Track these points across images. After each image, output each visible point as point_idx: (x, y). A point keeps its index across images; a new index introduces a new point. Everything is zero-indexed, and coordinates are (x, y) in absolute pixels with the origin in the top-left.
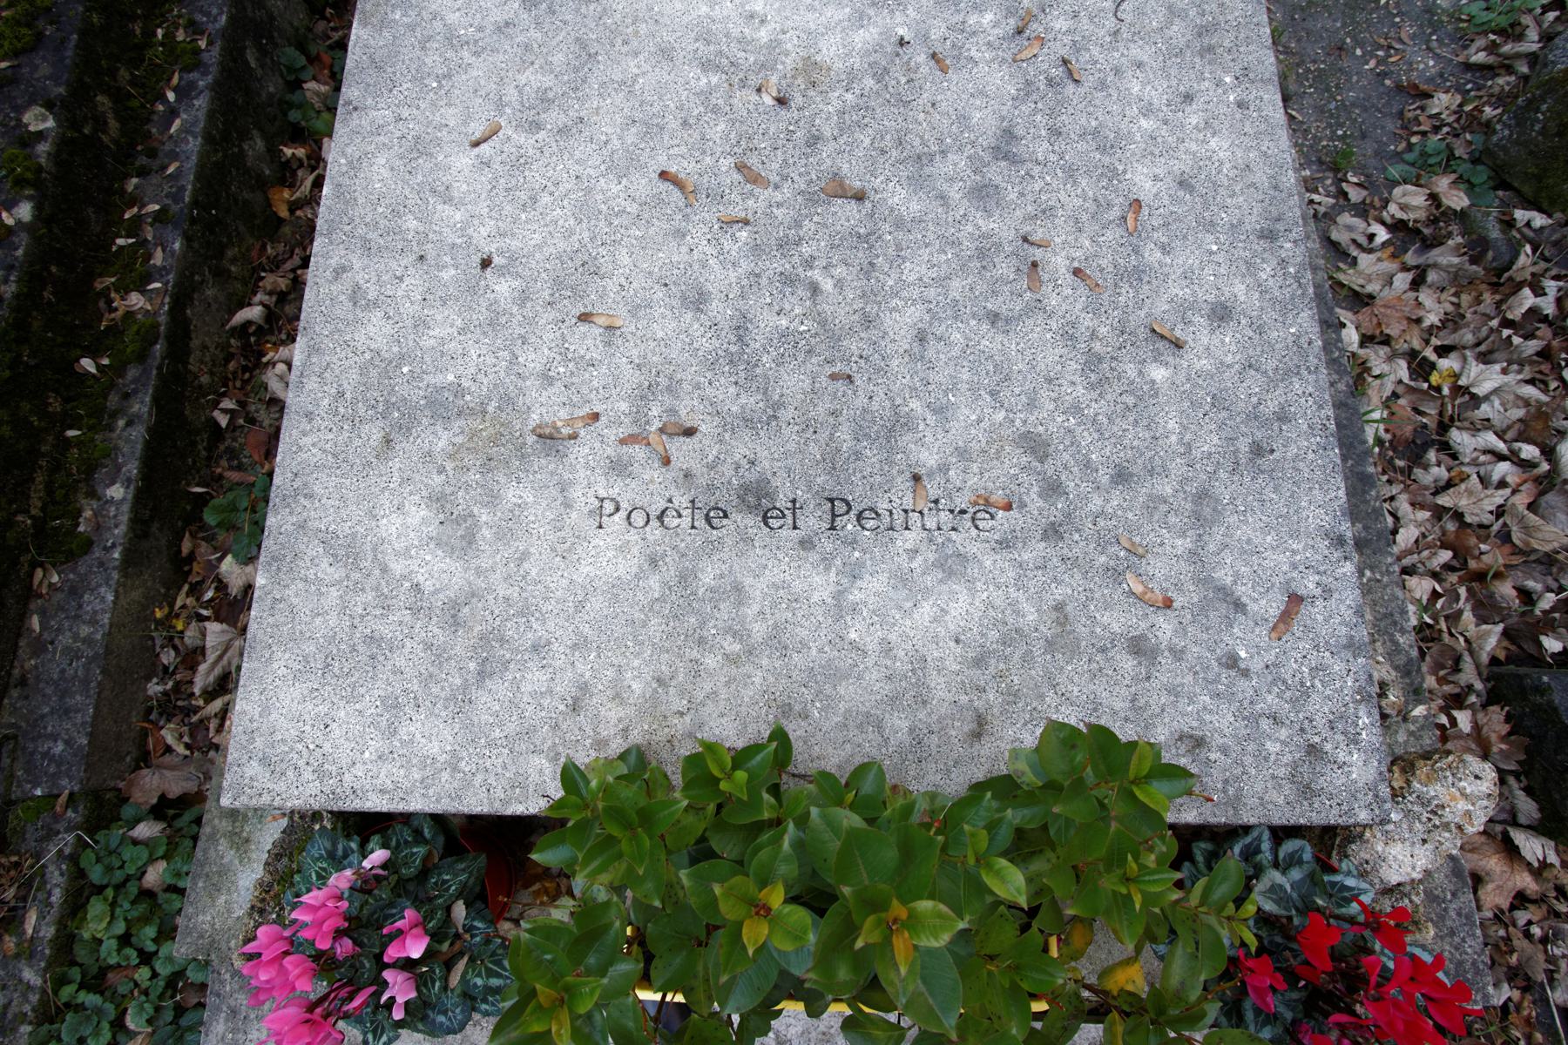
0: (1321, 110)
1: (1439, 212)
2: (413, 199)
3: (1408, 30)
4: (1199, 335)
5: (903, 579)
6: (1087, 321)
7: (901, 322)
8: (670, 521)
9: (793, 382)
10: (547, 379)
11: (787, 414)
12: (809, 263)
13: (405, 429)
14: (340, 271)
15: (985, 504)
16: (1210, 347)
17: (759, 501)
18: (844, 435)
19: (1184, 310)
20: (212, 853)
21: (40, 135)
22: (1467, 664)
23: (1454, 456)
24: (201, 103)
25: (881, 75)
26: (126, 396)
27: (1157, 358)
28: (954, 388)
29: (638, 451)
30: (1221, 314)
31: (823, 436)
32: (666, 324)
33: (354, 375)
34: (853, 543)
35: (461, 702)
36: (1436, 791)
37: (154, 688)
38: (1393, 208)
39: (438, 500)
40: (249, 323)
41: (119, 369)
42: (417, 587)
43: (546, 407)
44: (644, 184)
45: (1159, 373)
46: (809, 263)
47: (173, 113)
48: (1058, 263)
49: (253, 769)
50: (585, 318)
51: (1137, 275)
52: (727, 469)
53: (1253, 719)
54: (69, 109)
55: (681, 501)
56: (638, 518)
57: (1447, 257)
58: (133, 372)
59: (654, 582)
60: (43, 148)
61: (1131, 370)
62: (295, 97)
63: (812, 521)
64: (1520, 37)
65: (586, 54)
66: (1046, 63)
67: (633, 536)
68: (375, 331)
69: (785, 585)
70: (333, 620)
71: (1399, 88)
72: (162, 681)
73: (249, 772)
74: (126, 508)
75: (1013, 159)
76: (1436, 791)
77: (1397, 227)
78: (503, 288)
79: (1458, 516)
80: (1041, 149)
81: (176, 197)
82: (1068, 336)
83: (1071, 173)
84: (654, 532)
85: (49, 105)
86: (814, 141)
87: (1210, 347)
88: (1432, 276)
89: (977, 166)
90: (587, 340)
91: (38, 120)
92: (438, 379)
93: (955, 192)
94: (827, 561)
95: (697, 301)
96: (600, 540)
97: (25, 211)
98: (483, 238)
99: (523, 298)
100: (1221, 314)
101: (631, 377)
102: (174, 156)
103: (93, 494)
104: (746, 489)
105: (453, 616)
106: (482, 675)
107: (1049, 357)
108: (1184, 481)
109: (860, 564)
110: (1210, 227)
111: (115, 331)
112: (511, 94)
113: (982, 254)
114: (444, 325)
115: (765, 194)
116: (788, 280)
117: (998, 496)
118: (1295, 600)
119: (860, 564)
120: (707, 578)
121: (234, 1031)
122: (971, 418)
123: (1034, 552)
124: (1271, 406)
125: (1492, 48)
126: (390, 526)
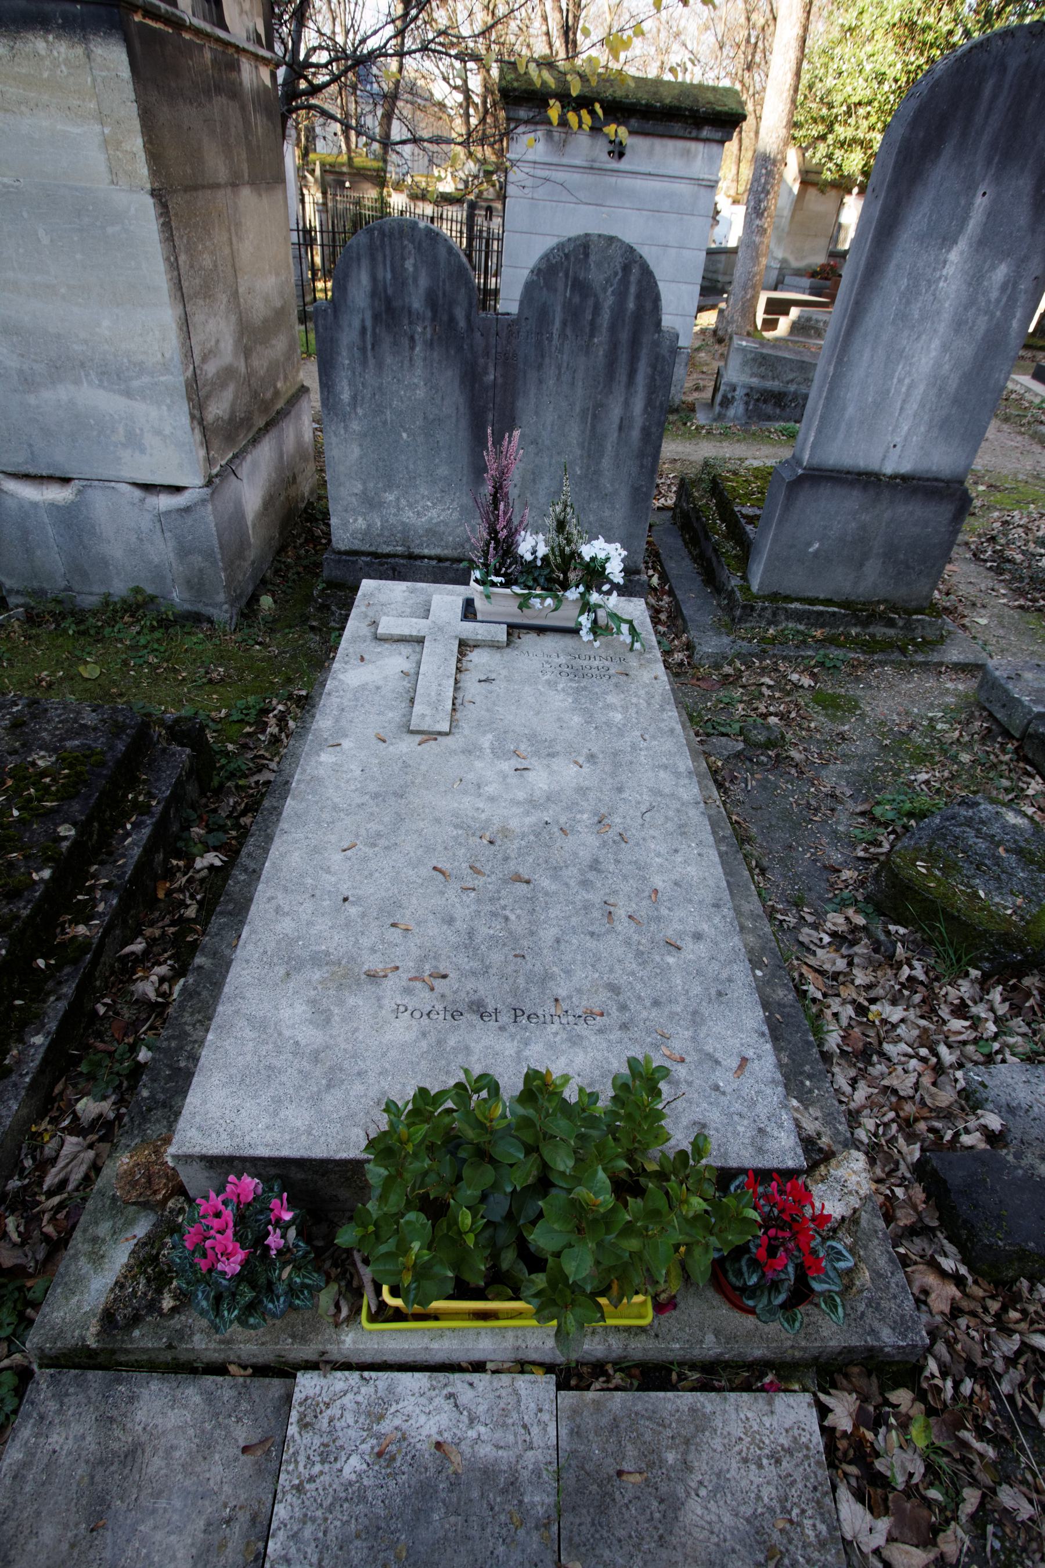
0: (784, 876)
1: (855, 929)
2: (311, 871)
3: (825, 840)
4: (688, 944)
5: (551, 1046)
6: (636, 937)
7: (548, 934)
8: (433, 1016)
9: (496, 957)
10: (373, 950)
11: (492, 971)
12: (504, 908)
13: (298, 969)
14: (270, 899)
15: (589, 1014)
16: (692, 950)
17: (479, 1009)
18: (521, 981)
19: (681, 934)
20: (73, 1267)
21: (66, 838)
22: (903, 1167)
23: (889, 1059)
24: (146, 831)
25: (537, 835)
26: (60, 983)
27: (669, 953)
28: (574, 962)
29: (418, 984)
30: (698, 937)
31: (511, 981)
32: (434, 930)
33: (273, 944)
34: (526, 1029)
35: (315, 1100)
36: (839, 1173)
37: (14, 1184)
38: (829, 925)
39: (312, 1002)
40: (133, 953)
41: (58, 967)
42: (297, 1043)
43: (373, 962)
44: (425, 871)
45: (671, 960)
46: (504, 908)
47: (128, 834)
48: (621, 913)
49: (193, 1132)
50: (394, 925)
51: (658, 919)
52: (463, 995)
53: (730, 1115)
54: (83, 829)
55: (439, 1007)
56: (417, 1014)
57: (861, 950)
58: (67, 970)
59: (424, 1044)
60: (65, 844)
61: (658, 958)
62: (185, 834)
63: (505, 1018)
64: (880, 845)
65: (400, 818)
66: (612, 834)
67: (414, 1022)
68: (286, 926)
69: (490, 1047)
70: (249, 1057)
71: (825, 867)
72: (21, 1178)
73: (189, 1134)
74: (42, 1050)
75: (599, 871)
76: (839, 1173)
77: (834, 934)
78: (353, 911)
79: (895, 1092)
80: (611, 868)
81: (119, 877)
82: (627, 942)
83: (625, 878)
84: (425, 1020)
85: (74, 824)
86: (506, 859)
87: (692, 950)
88: (856, 960)
89: (582, 872)
90: (395, 935)
91: (66, 830)
92: (317, 948)
93: (572, 883)
94: (512, 1037)
95: (450, 921)
96: (397, 1023)
97: (46, 874)
98: (345, 889)
99: (363, 915)
100: (698, 937)
101: (415, 952)
102: (124, 856)
103: (21, 1040)
104: (472, 1003)
105: (316, 1057)
106: (329, 1086)
107: (619, 951)
108: (686, 1006)
109: (529, 1038)
110: (690, 901)
111: (63, 945)
112: (363, 832)
113: (585, 908)
114: (322, 925)
115: (483, 879)
116: (494, 914)
117: (596, 1010)
118: (744, 1060)
119: (529, 1038)
120: (452, 1042)
121: (37, 1436)
122: (582, 975)
123: (615, 1035)
124: (724, 976)
125: (866, 850)
126: (285, 1013)
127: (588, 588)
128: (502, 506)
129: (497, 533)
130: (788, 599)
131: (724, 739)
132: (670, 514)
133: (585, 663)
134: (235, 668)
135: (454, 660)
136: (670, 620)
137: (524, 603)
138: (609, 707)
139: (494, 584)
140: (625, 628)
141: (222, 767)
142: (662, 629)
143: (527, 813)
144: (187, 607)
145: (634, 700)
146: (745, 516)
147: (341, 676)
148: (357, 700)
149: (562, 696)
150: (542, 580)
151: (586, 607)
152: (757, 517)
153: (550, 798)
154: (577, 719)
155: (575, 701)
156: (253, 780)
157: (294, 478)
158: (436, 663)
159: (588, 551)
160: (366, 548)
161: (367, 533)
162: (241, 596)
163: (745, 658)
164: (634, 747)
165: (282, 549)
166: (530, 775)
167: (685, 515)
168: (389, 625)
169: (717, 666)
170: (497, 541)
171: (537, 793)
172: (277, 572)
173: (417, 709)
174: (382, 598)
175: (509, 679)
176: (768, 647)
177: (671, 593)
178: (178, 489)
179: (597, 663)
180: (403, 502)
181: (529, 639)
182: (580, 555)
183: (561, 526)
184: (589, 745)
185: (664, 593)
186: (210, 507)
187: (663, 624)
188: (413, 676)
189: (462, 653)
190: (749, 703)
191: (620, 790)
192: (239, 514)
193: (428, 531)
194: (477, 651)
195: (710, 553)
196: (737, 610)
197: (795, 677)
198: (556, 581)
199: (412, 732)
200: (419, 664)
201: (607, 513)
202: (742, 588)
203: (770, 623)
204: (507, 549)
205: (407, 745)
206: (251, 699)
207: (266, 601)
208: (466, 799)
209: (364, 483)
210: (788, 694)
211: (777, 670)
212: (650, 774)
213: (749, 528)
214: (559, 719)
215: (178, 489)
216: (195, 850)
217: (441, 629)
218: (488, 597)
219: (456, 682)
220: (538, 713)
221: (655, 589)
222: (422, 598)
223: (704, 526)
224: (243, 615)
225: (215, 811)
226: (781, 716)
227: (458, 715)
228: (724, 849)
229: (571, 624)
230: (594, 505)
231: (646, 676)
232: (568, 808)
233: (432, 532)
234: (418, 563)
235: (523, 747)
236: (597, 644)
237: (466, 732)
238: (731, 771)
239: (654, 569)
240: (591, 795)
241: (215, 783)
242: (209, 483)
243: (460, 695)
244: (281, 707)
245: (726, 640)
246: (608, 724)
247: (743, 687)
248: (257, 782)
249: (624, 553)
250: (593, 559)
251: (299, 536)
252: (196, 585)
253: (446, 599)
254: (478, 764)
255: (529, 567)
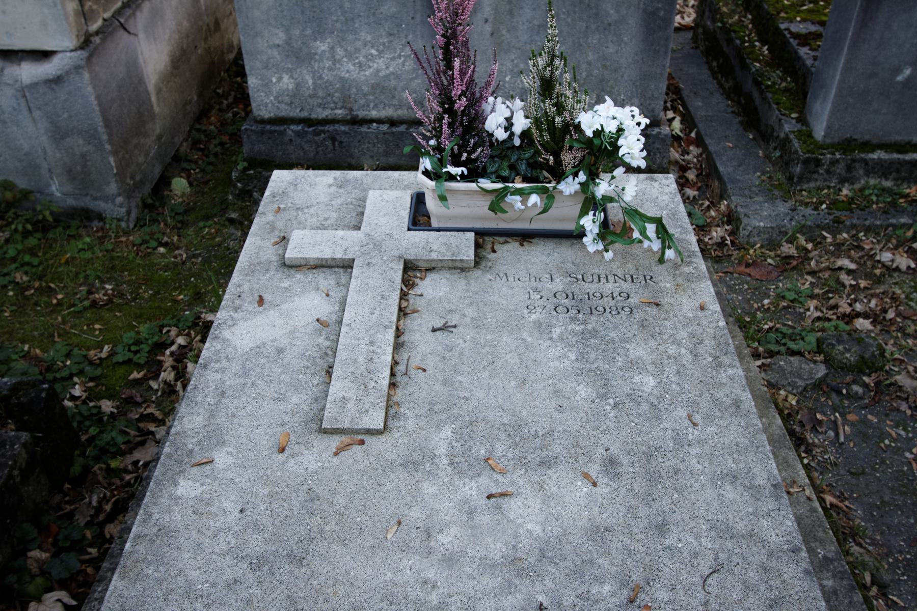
127: (593, 176)
128: (457, 63)
129: (452, 102)
130: (867, 146)
131: (795, 360)
132: (690, 35)
133: (593, 288)
134: (129, 283)
135: (396, 296)
136: (704, 186)
137: (497, 202)
138: (634, 365)
139: (451, 178)
140: (651, 229)
141: (92, 439)
142: (691, 192)
143: (509, 588)
144: (71, 202)
145: (672, 350)
146: (796, 36)
147: (227, 334)
148: (246, 374)
149: (557, 350)
150: (523, 167)
151: (590, 203)
152: (818, 36)
153: (546, 553)
154: (584, 391)
155: (581, 356)
156: (129, 460)
157: (217, 24)
158: (370, 299)
159: (589, 122)
160: (296, 113)
161: (295, 94)
162: (142, 182)
163: (812, 233)
164: (678, 438)
165: (203, 115)
166: (513, 506)
167: (710, 36)
168: (305, 244)
169: (772, 245)
170: (451, 112)
171: (525, 543)
172: (195, 144)
173: (337, 388)
174: (299, 198)
175: (477, 325)
176: (843, 215)
177: (699, 142)
178: (44, 55)
179: (609, 287)
180: (340, 52)
181: (508, 251)
182: (578, 127)
183: (547, 86)
184: (605, 440)
185: (690, 142)
186: (86, 75)
187: (692, 185)
188: (331, 327)
189: (408, 283)
190: (824, 298)
191: (662, 529)
192: (135, 78)
193: (374, 87)
194: (431, 276)
195: (749, 86)
196: (794, 166)
197: (886, 257)
198: (545, 166)
199: (326, 432)
200: (343, 303)
201: (612, 49)
202: (800, 135)
203: (843, 181)
204: (469, 124)
205: (316, 457)
206: (144, 328)
207: (180, 184)
208: (408, 562)
209: (287, 31)
210: (878, 281)
211: (859, 248)
212: (709, 492)
213: (803, 51)
214: (557, 393)
215: (44, 55)
216: (31, 588)
217: (378, 246)
218: (443, 198)
219: (399, 333)
220: (523, 383)
221: (677, 138)
222: (356, 193)
223: (739, 51)
224: (145, 206)
225: (70, 515)
226: (873, 317)
227: (399, 395)
228: (829, 583)
229: (570, 226)
230: (594, 40)
231: (686, 306)
232: (577, 574)
233: (379, 88)
234: (364, 129)
235: (500, 450)
236: (609, 255)
237: (411, 426)
238: (812, 412)
239: (675, 109)
240: (615, 543)
241: (76, 469)
242: (86, 43)
243: (403, 357)
244: (181, 341)
245: (783, 208)
246: (634, 397)
247: (812, 273)
248: (136, 463)
249: (645, 121)
250: (598, 133)
251: (225, 96)
252: (80, 174)
253: (387, 195)
254: (428, 488)
255: (503, 150)
